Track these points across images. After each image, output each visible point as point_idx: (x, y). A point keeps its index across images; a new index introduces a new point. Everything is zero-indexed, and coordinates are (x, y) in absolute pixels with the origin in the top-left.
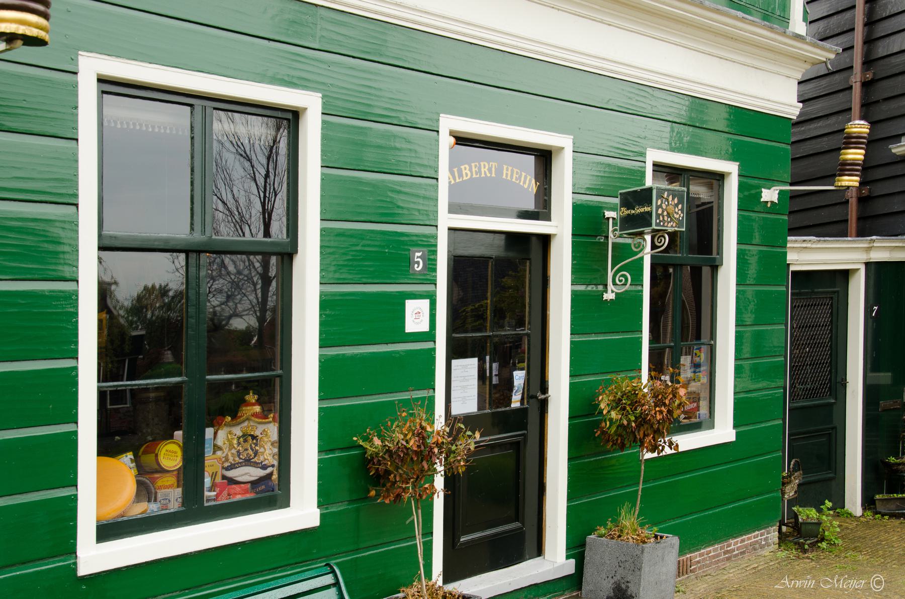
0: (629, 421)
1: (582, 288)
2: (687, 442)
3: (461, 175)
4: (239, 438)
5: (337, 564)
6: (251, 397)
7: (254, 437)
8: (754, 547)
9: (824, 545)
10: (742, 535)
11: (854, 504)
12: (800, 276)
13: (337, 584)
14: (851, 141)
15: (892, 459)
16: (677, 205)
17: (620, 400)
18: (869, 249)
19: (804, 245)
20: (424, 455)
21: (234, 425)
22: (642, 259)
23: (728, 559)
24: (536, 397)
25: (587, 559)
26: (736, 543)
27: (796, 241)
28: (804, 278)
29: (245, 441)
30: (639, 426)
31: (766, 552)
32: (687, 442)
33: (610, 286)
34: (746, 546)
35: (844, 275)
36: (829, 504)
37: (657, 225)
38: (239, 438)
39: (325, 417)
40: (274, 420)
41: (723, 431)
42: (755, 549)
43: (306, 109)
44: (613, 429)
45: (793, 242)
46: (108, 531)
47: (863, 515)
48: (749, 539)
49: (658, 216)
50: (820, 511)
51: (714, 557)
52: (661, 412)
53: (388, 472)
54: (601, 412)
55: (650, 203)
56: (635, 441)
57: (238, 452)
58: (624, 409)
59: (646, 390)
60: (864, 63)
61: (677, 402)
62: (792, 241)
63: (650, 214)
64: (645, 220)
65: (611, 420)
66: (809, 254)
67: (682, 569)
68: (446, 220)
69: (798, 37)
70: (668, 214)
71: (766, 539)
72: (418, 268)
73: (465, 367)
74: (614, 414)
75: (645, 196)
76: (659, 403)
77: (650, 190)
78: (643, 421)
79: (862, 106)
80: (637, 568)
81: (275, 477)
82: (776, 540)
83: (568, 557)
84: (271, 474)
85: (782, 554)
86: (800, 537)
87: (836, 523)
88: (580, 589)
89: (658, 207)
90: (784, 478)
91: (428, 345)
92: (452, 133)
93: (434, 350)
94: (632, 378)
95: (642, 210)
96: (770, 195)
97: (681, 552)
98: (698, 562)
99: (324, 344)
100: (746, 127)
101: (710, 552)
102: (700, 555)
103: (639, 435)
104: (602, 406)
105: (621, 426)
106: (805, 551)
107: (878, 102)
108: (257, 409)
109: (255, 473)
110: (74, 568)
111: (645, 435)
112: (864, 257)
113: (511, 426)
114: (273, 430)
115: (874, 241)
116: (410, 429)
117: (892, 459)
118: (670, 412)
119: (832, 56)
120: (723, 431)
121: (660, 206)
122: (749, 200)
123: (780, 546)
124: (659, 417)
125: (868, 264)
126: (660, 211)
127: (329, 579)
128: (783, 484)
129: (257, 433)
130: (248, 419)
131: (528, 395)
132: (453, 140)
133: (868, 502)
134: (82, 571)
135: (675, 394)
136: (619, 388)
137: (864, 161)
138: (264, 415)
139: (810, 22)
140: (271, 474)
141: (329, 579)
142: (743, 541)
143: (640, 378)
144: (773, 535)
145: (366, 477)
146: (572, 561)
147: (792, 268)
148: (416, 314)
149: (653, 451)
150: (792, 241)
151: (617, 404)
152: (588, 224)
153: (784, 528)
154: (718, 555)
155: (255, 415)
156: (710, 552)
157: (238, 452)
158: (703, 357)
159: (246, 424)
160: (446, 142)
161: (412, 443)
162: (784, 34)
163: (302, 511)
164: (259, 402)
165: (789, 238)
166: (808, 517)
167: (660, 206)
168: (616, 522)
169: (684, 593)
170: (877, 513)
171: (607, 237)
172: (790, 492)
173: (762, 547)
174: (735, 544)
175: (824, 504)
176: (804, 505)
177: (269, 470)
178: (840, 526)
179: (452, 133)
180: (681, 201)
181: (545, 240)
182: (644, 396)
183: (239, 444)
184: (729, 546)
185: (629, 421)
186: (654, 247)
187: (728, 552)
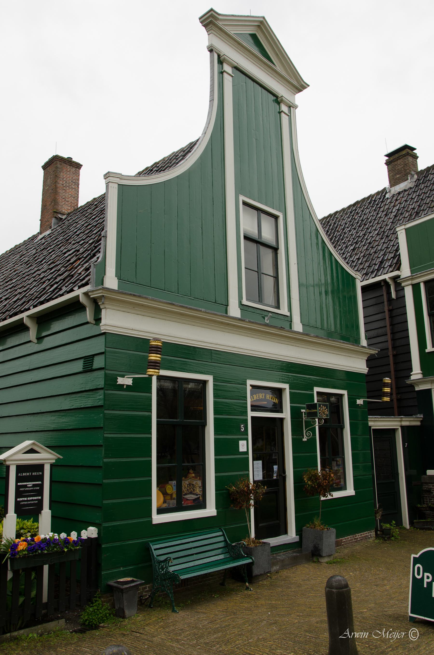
0: (315, 485)
1: (295, 437)
2: (337, 494)
3: (253, 398)
4: (188, 485)
5: (224, 529)
6: (191, 471)
7: (193, 485)
8: (366, 538)
9: (393, 538)
10: (360, 533)
11: (406, 523)
12: (376, 431)
13: (223, 535)
14: (386, 385)
15: (419, 505)
16: (325, 409)
17: (311, 477)
18: (401, 421)
19: (376, 419)
20: (245, 494)
21: (186, 480)
22: (315, 427)
23: (356, 542)
24: (282, 475)
25: (303, 536)
26: (358, 536)
27: (372, 418)
28: (378, 432)
29: (190, 486)
30: (318, 487)
31: (371, 540)
32: (337, 494)
33: (305, 436)
34: (363, 537)
35: (393, 431)
36: (394, 522)
37: (320, 416)
38: (188, 485)
39: (217, 479)
40: (200, 479)
41: (350, 491)
42: (366, 539)
43: (208, 381)
44: (309, 488)
45: (370, 418)
46: (160, 511)
47: (410, 529)
48: (364, 534)
49: (319, 413)
50: (391, 525)
51: (350, 540)
52: (326, 482)
53: (237, 499)
54: (305, 482)
55: (316, 409)
56: (317, 493)
57: (188, 489)
58: (313, 481)
59: (320, 474)
60: (392, 348)
61: (331, 479)
62: (370, 418)
63: (317, 412)
64: (315, 414)
65: (308, 484)
66: (377, 423)
67: (338, 544)
68: (251, 414)
69: (363, 347)
70: (323, 413)
71: (370, 535)
72: (243, 430)
73: (258, 463)
74: (309, 482)
75: (314, 406)
76: (325, 479)
77: (316, 404)
78: (319, 485)
79: (394, 364)
80: (321, 539)
81: (201, 498)
82: (374, 535)
83: (296, 535)
84: (199, 497)
85: (377, 541)
86: (384, 535)
87: (397, 530)
88: (301, 547)
89: (319, 410)
90: (376, 511)
91: (246, 456)
92: (251, 386)
93: (248, 457)
94: (315, 470)
95: (314, 411)
96: (360, 402)
97: (337, 537)
98: (344, 542)
99: (216, 455)
100: (349, 378)
101: (348, 538)
102: (345, 539)
103: (319, 490)
104: (305, 479)
105: (312, 487)
106: (386, 540)
107: (399, 363)
108: (193, 475)
109: (194, 497)
110: (151, 521)
111: (321, 490)
112: (399, 424)
113: (273, 485)
114: (199, 483)
115: (402, 418)
116: (244, 485)
117: (419, 505)
118: (329, 482)
119: (377, 352)
120: (350, 491)
121: (320, 410)
122: (352, 404)
123: (376, 538)
124: (325, 484)
125: (402, 427)
126: (320, 411)
127: (221, 533)
128: (376, 513)
129: (194, 483)
130: (190, 478)
131: (279, 475)
132: (251, 387)
133: (411, 523)
134: (154, 522)
135: (330, 476)
136: (310, 473)
137: (390, 392)
138: (196, 477)
139: (368, 339)
140: (199, 497)
141: (221, 533)
142: (361, 535)
143: (317, 469)
144: (373, 533)
145: (230, 498)
146: (298, 536)
147: (372, 428)
148: (243, 446)
149: (324, 497)
150: (370, 418)
151: (310, 479)
152: (295, 414)
153: (379, 532)
154: (352, 540)
155: (193, 477)
156: (348, 538)
157: (188, 489)
158: (340, 462)
159: (190, 480)
160: (249, 388)
161: (245, 489)
162: (358, 346)
163: (210, 510)
164: (194, 473)
165: (369, 416)
166: (386, 527)
167: (320, 410)
168: (313, 523)
169: (340, 553)
170: (415, 528)
171: (302, 419)
172: (379, 517)
173: (369, 538)
174: (358, 536)
175: (392, 522)
176: (385, 523)
177: (199, 496)
178: (398, 531)
179: (251, 386)
180: (327, 408)
181: (282, 420)
182: (320, 476)
183: (188, 487)
184: (356, 536)
185: (315, 485)
186: (319, 423)
187: (355, 539)
